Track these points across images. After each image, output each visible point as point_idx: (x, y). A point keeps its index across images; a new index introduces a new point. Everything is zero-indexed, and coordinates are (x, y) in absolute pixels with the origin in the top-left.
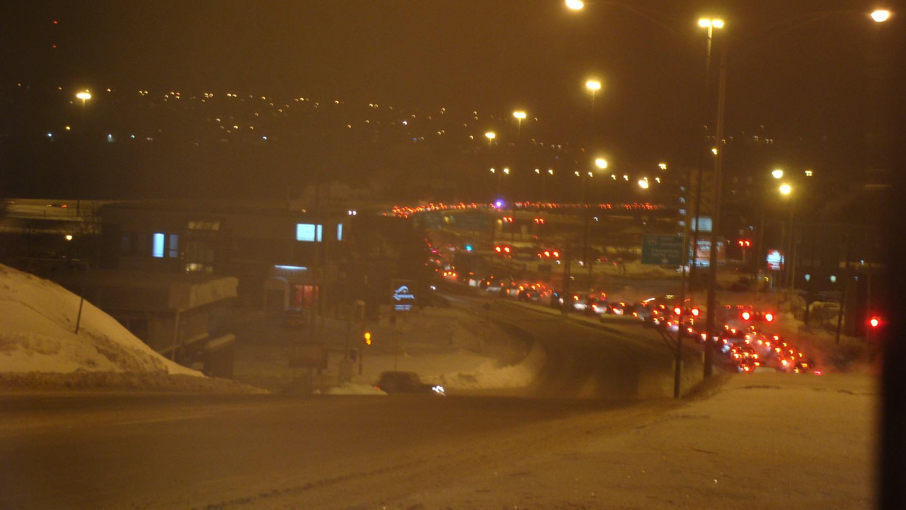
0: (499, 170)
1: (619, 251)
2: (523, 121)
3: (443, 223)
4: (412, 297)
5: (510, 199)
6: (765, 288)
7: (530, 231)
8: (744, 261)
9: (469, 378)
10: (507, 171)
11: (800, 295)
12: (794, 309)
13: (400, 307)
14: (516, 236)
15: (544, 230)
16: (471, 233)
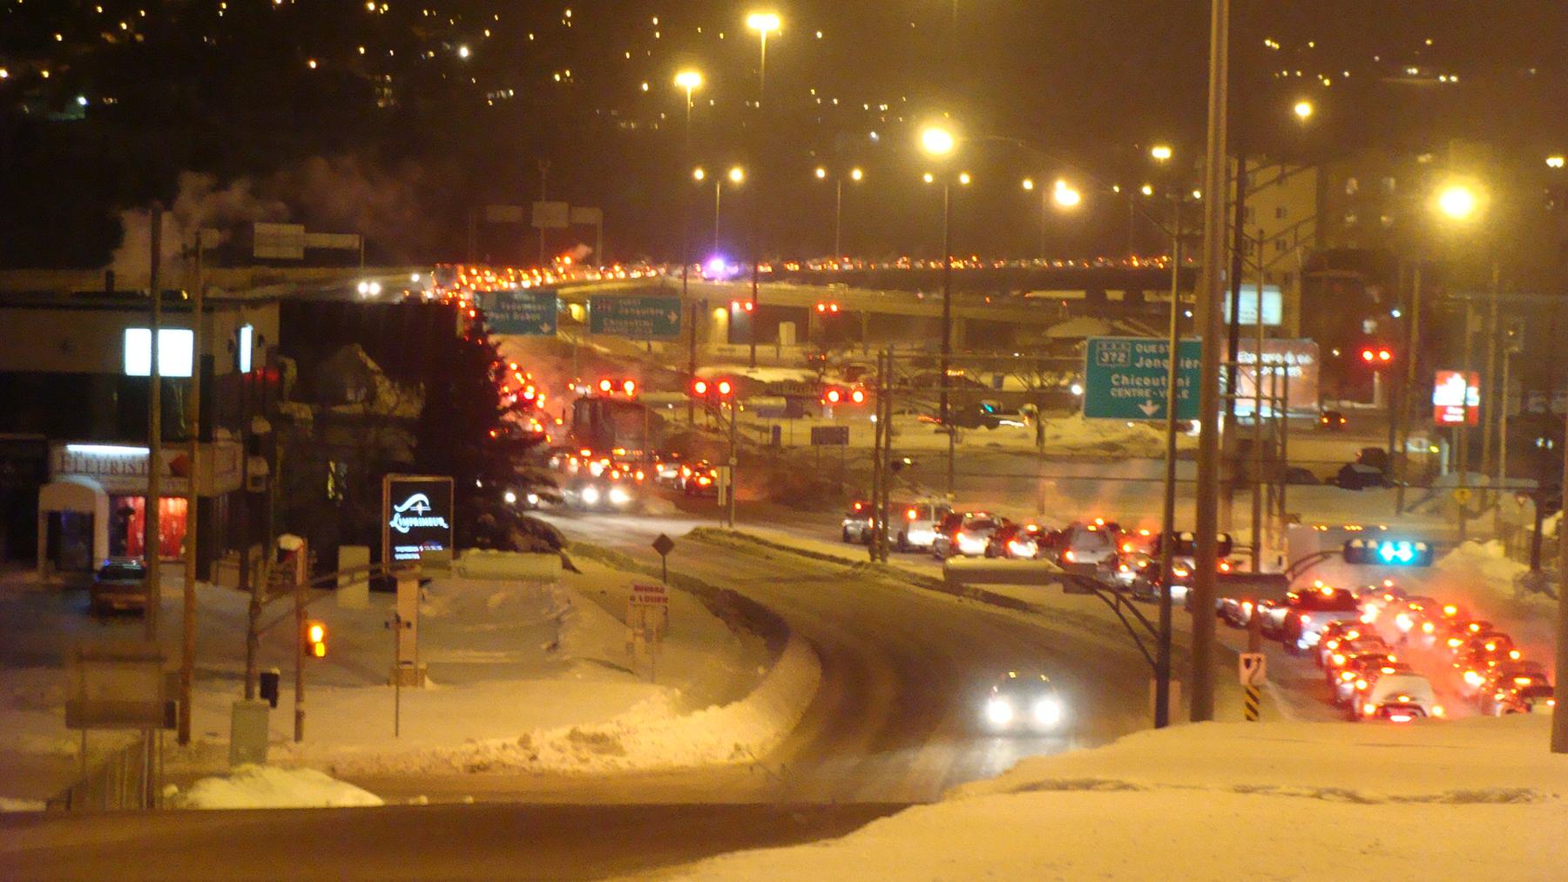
0: (717, 172)
1: (1031, 386)
2: (774, 46)
3: (567, 321)
4: (439, 522)
5: (745, 250)
6: (1429, 474)
7: (802, 336)
8: (1377, 404)
9: (600, 742)
10: (737, 175)
11: (1522, 492)
12: (1504, 532)
13: (407, 553)
14: (763, 350)
15: (841, 330)
16: (643, 345)
